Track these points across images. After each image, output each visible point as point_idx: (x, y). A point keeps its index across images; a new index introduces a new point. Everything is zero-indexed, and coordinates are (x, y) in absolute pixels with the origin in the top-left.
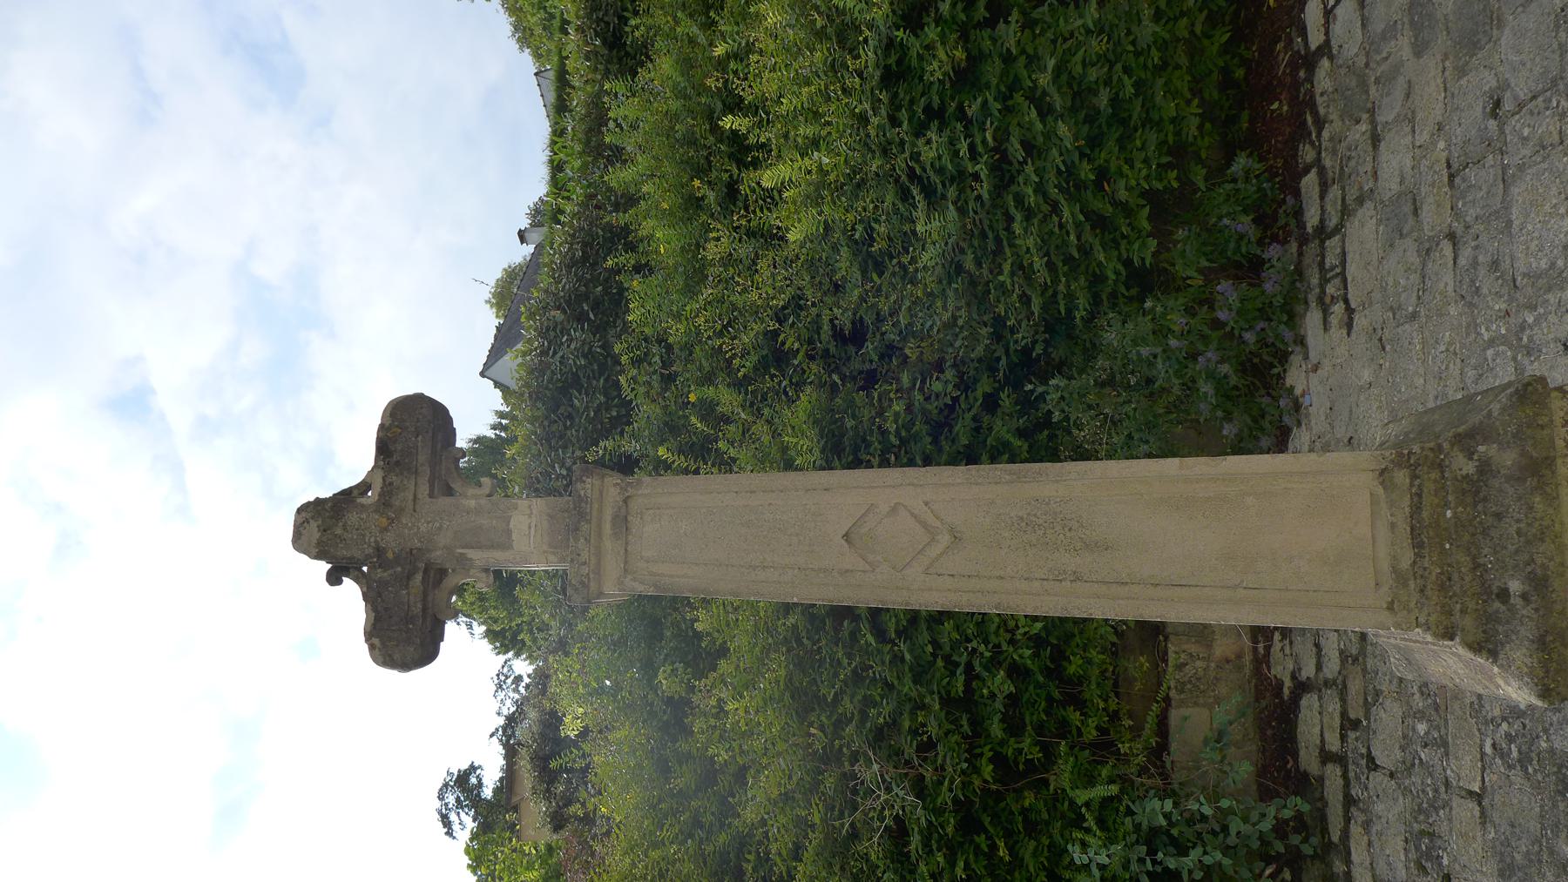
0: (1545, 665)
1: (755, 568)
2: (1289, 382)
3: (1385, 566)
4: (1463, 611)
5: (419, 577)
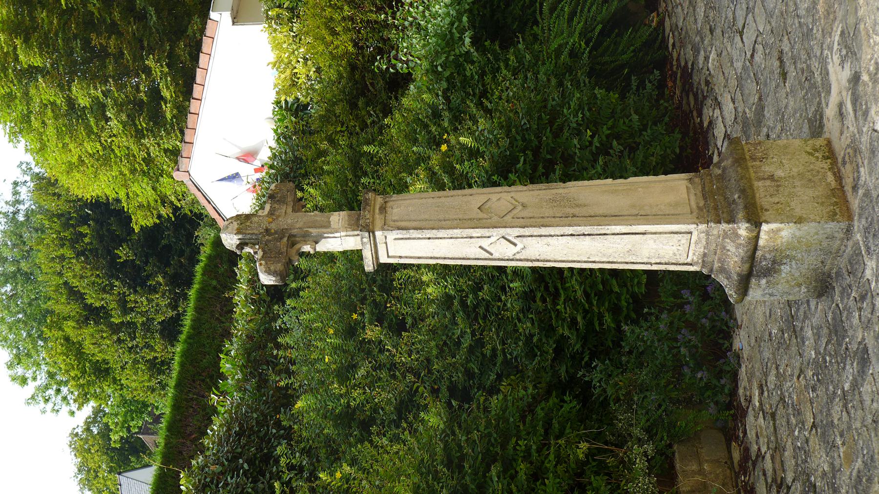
0: (747, 213)
1: (441, 221)
2: (737, 345)
3: (694, 206)
4: (723, 213)
5: (286, 239)
